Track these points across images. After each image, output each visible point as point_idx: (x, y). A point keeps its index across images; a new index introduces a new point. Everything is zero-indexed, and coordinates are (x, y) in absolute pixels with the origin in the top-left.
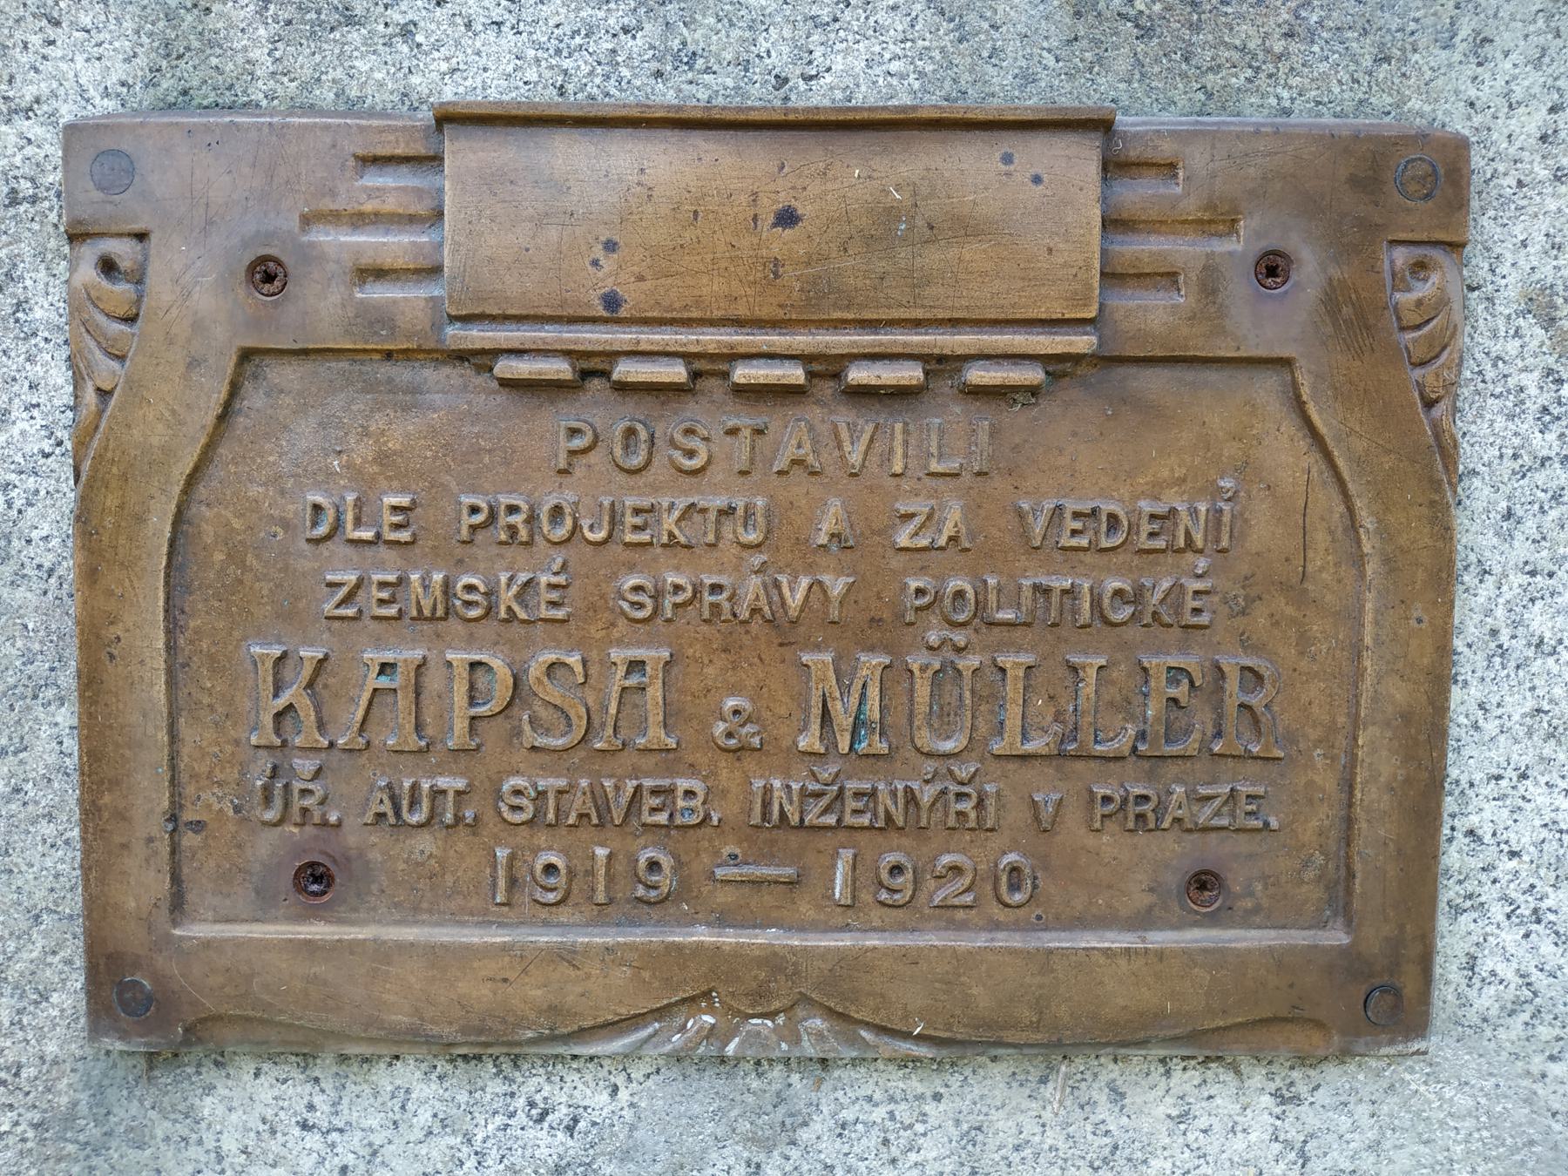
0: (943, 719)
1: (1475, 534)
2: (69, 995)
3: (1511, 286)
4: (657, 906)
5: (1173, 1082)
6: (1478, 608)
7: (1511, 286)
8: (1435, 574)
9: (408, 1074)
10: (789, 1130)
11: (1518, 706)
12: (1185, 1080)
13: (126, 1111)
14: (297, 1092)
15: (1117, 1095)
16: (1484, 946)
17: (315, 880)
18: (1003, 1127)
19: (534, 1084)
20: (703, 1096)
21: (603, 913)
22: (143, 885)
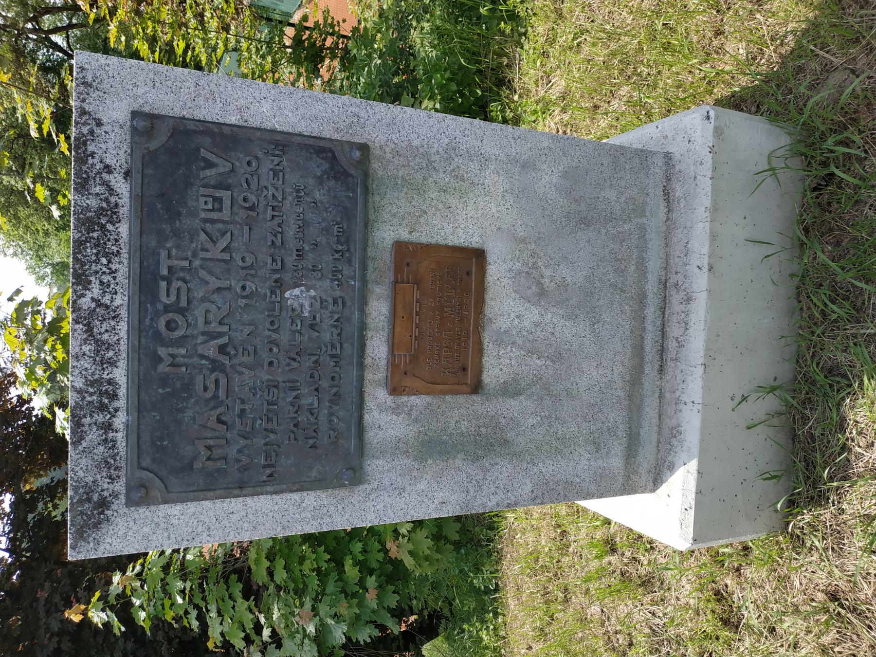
0: (451, 302)
1: (433, 241)
2: (474, 397)
3: (408, 236)
4: (468, 332)
5: (526, 47)
6: (441, 242)
7: (408, 236)
8: (438, 247)
9: (483, 360)
10: (491, 319)
11: (451, 237)
12: (487, 275)
13: (486, 392)
14: (485, 373)
15: (55, 469)
16: (475, 242)
17: (464, 369)
18: (491, 295)
19: (485, 347)
20: (487, 328)
21: (469, 338)
22: (465, 388)
